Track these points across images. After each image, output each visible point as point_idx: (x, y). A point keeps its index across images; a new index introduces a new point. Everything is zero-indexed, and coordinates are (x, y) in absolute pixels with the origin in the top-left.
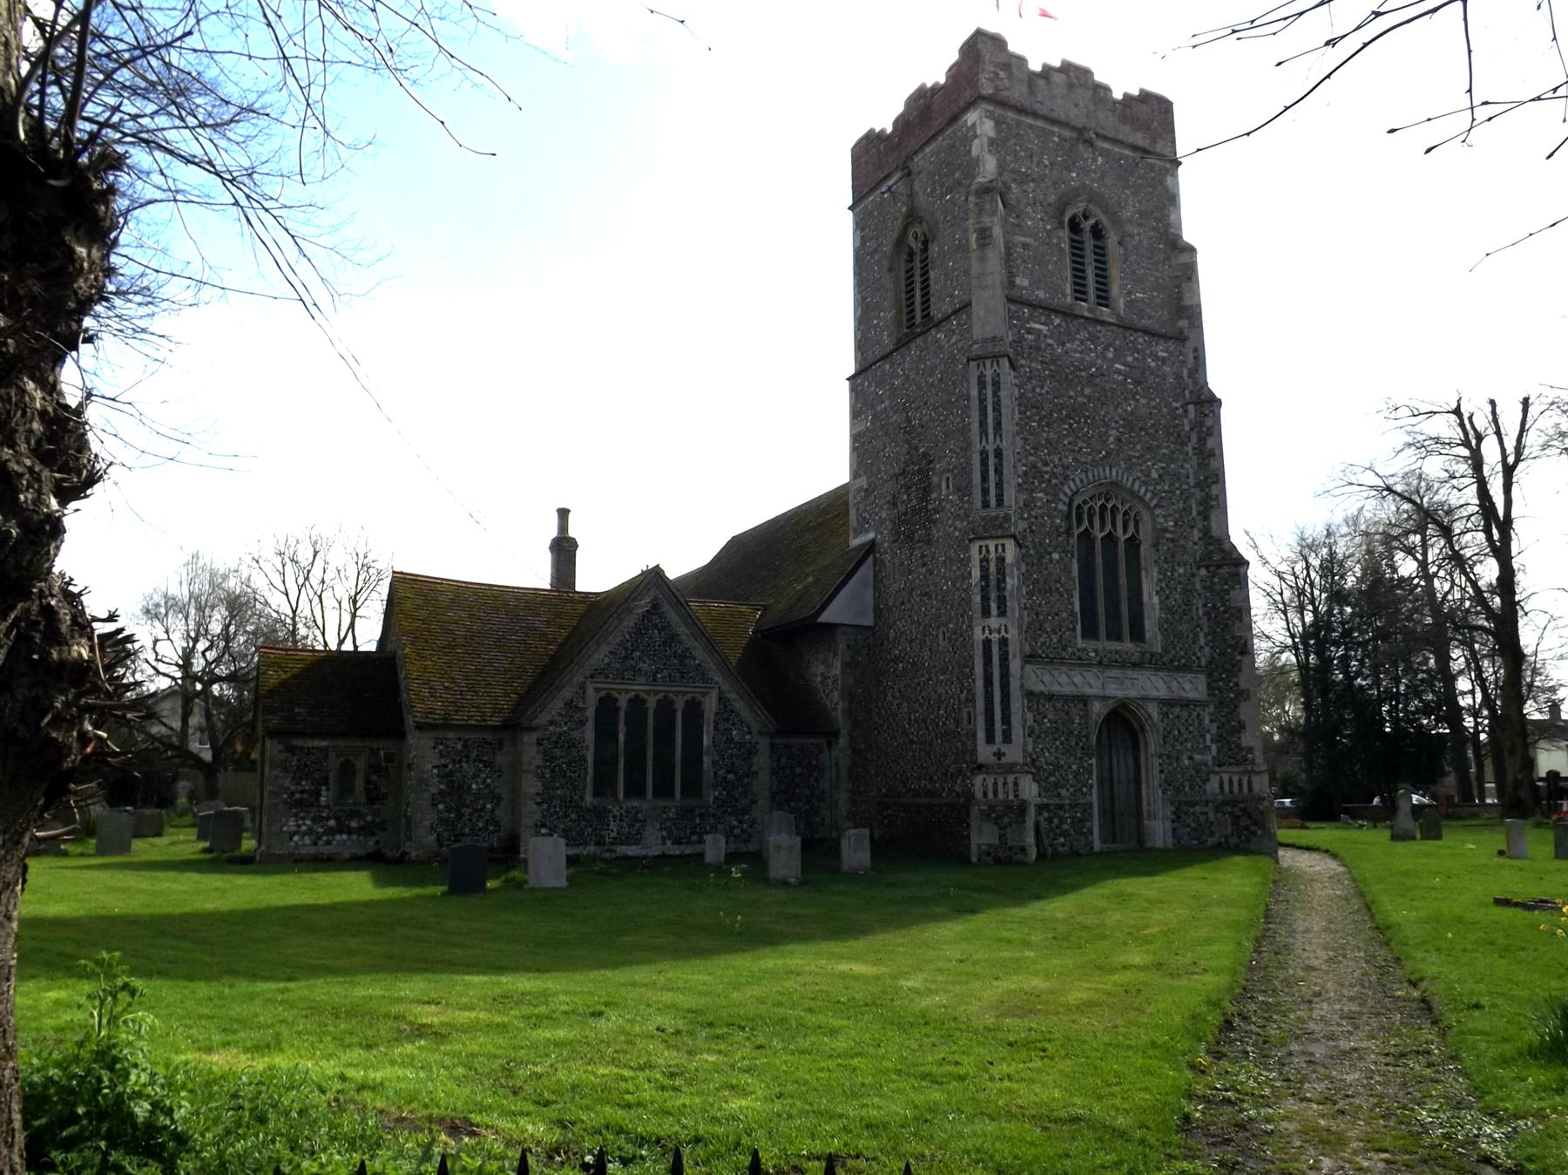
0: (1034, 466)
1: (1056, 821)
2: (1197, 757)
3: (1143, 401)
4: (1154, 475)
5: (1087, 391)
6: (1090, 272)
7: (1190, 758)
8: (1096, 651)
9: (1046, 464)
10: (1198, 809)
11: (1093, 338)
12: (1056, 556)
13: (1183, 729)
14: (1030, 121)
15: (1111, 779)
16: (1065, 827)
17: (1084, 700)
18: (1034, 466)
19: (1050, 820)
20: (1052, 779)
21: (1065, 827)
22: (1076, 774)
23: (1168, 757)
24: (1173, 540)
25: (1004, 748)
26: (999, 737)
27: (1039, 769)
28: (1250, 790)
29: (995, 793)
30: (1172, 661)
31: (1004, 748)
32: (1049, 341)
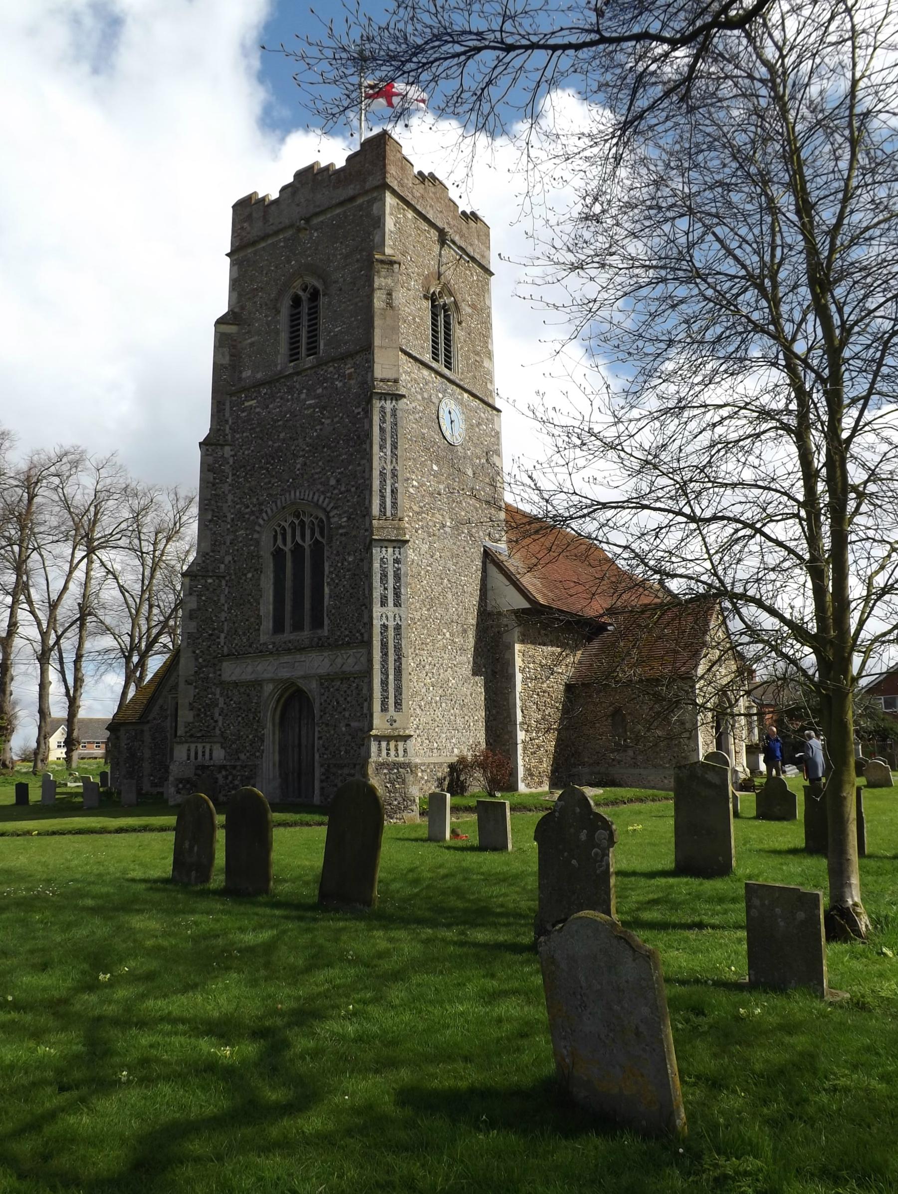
0: (239, 511)
1: (230, 778)
2: (354, 724)
3: (328, 421)
4: (333, 482)
5: (282, 435)
6: (304, 334)
7: (348, 725)
8: (274, 643)
9: (248, 507)
10: (346, 771)
11: (291, 390)
12: (249, 575)
13: (341, 700)
14: (263, 245)
15: (300, 745)
16: (236, 782)
17: (257, 684)
18: (239, 511)
19: (226, 777)
20: (234, 746)
21: (236, 782)
22: (252, 743)
23: (327, 725)
24: (345, 534)
25: (396, 716)
26: (391, 707)
27: (225, 738)
28: (211, 759)
29: (196, 758)
30: (336, 640)
31: (396, 716)
32: (258, 410)
